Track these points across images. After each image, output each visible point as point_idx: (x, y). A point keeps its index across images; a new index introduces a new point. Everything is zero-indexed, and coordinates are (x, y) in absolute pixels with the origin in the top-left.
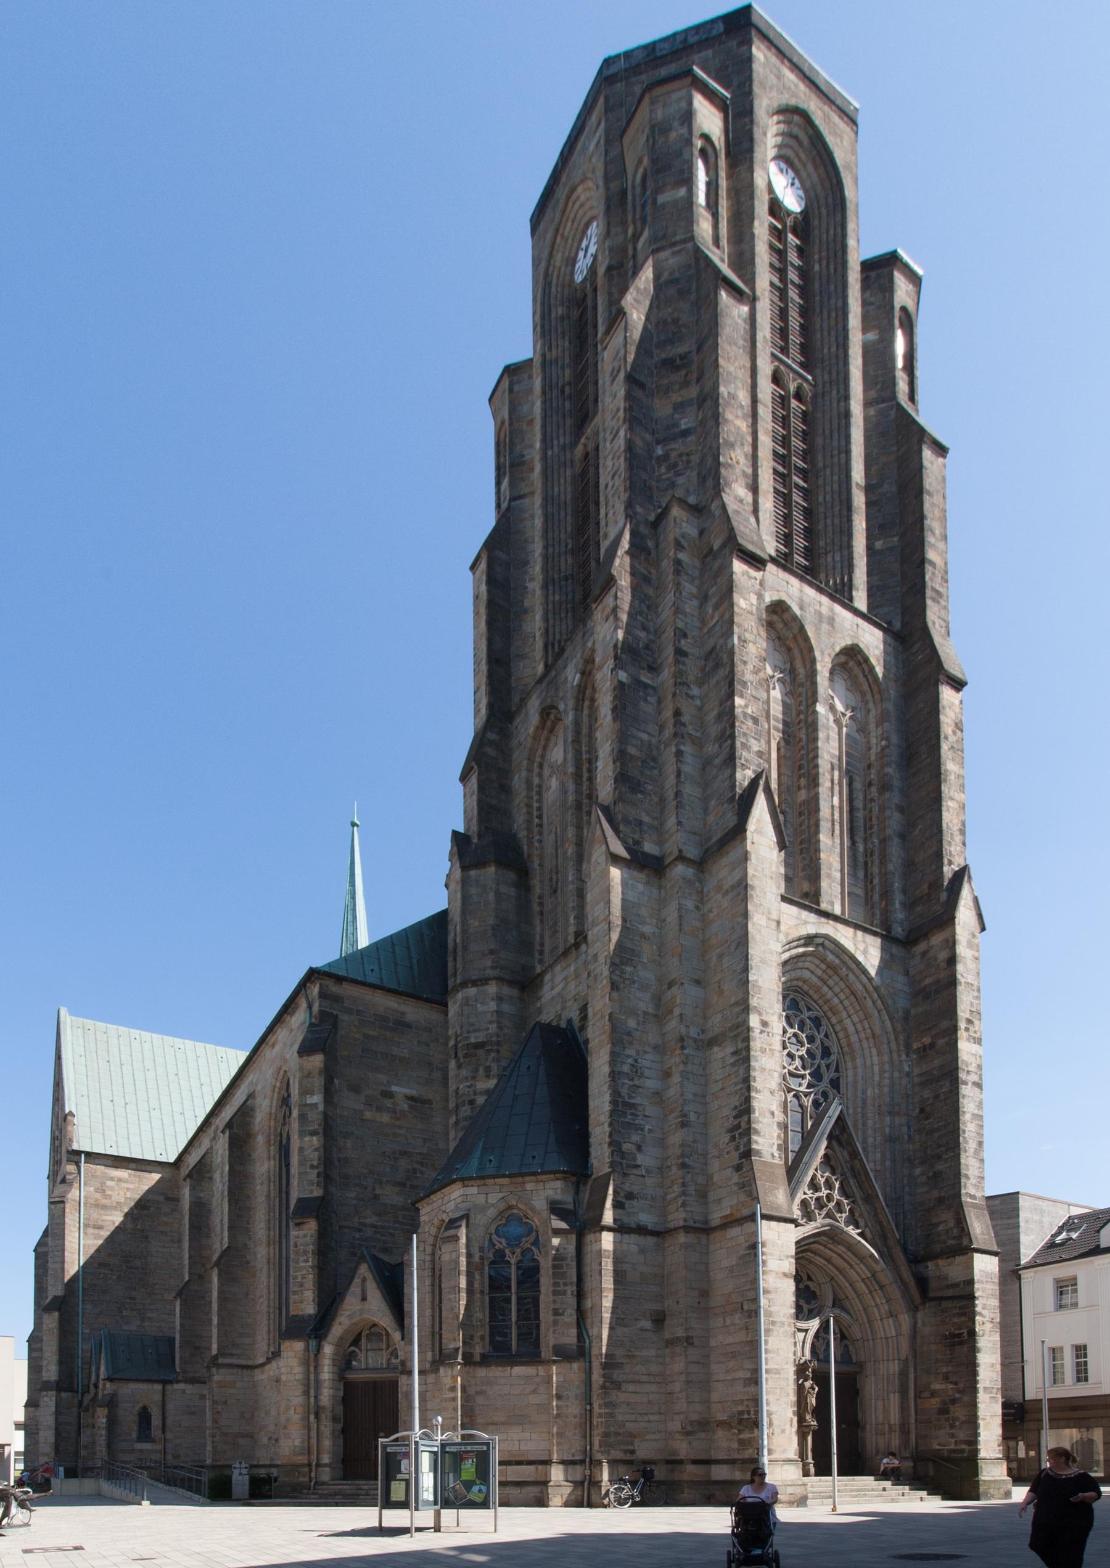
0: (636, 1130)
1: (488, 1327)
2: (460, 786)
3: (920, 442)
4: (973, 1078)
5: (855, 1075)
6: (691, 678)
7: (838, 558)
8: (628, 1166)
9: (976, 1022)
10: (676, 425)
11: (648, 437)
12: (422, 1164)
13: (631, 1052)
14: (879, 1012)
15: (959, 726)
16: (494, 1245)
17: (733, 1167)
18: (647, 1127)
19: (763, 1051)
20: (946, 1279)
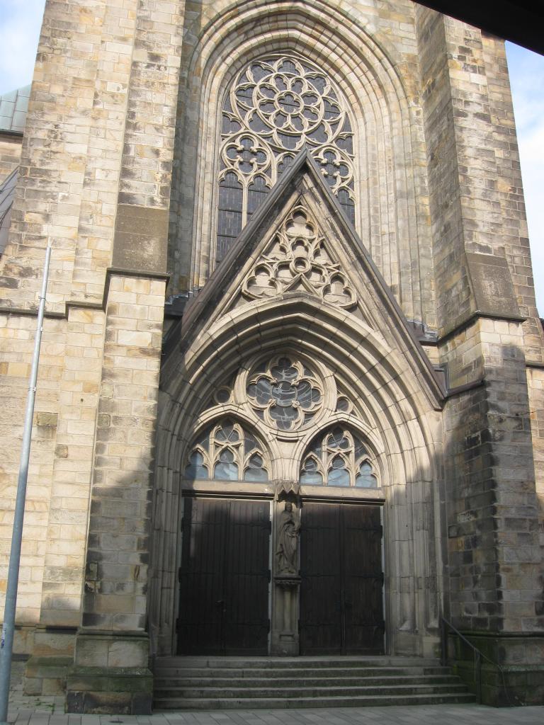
0: (46, 197)
8: (29, 238)
13: (52, 118)
14: (380, 61)
18: (61, 195)
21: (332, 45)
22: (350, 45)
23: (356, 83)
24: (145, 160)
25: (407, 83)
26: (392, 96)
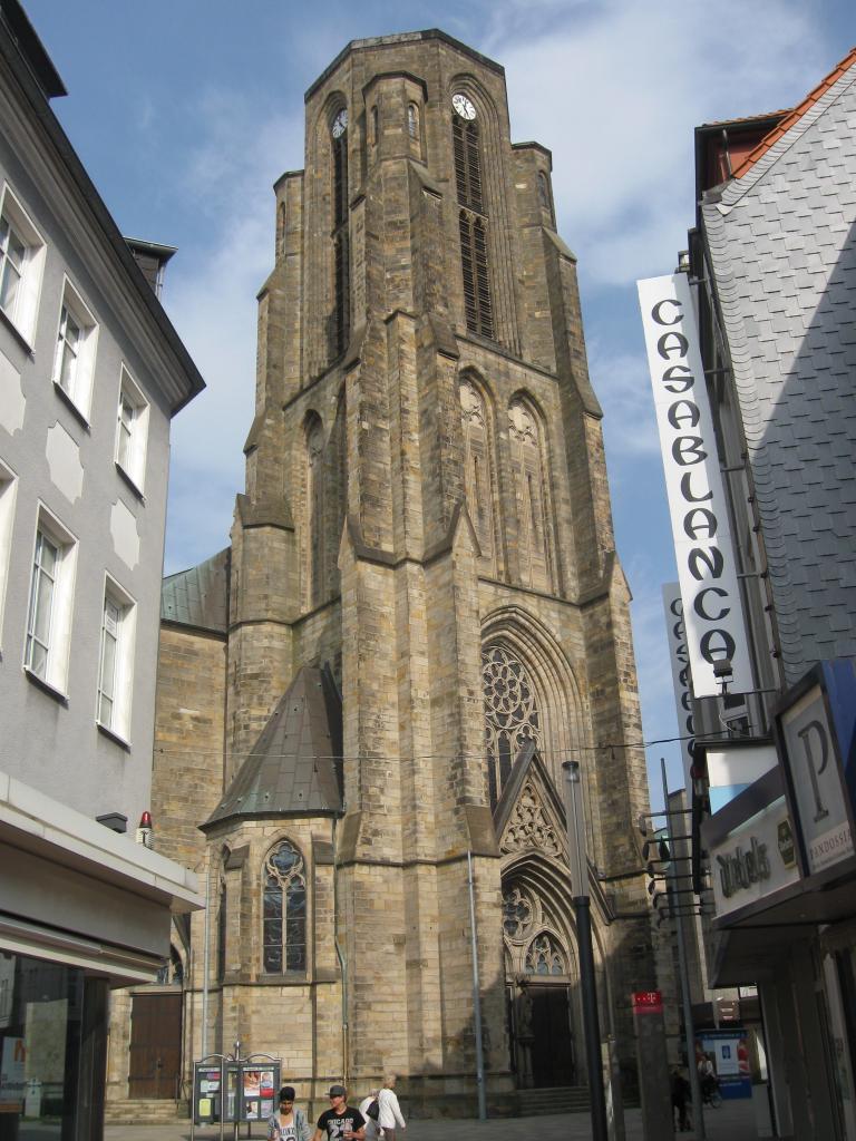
0: (380, 775)
1: (262, 949)
2: (245, 456)
3: (558, 255)
4: (634, 720)
5: (549, 712)
6: (412, 427)
7: (510, 326)
9: (632, 675)
10: (398, 261)
11: (381, 268)
12: (202, 779)
13: (375, 710)
15: (600, 445)
16: (269, 873)
17: (452, 810)
19: (471, 715)
20: (627, 897)
21: (525, 639)
22: (542, 646)
23: (543, 674)
24: (475, 772)
25: (581, 682)
26: (569, 691)
